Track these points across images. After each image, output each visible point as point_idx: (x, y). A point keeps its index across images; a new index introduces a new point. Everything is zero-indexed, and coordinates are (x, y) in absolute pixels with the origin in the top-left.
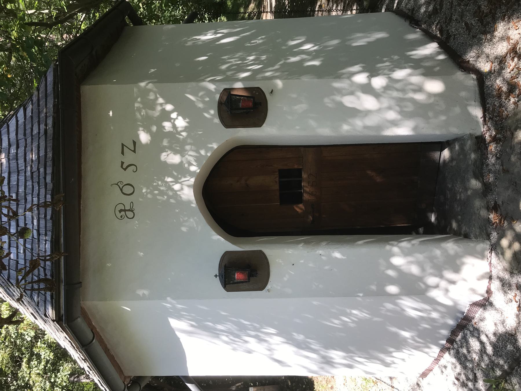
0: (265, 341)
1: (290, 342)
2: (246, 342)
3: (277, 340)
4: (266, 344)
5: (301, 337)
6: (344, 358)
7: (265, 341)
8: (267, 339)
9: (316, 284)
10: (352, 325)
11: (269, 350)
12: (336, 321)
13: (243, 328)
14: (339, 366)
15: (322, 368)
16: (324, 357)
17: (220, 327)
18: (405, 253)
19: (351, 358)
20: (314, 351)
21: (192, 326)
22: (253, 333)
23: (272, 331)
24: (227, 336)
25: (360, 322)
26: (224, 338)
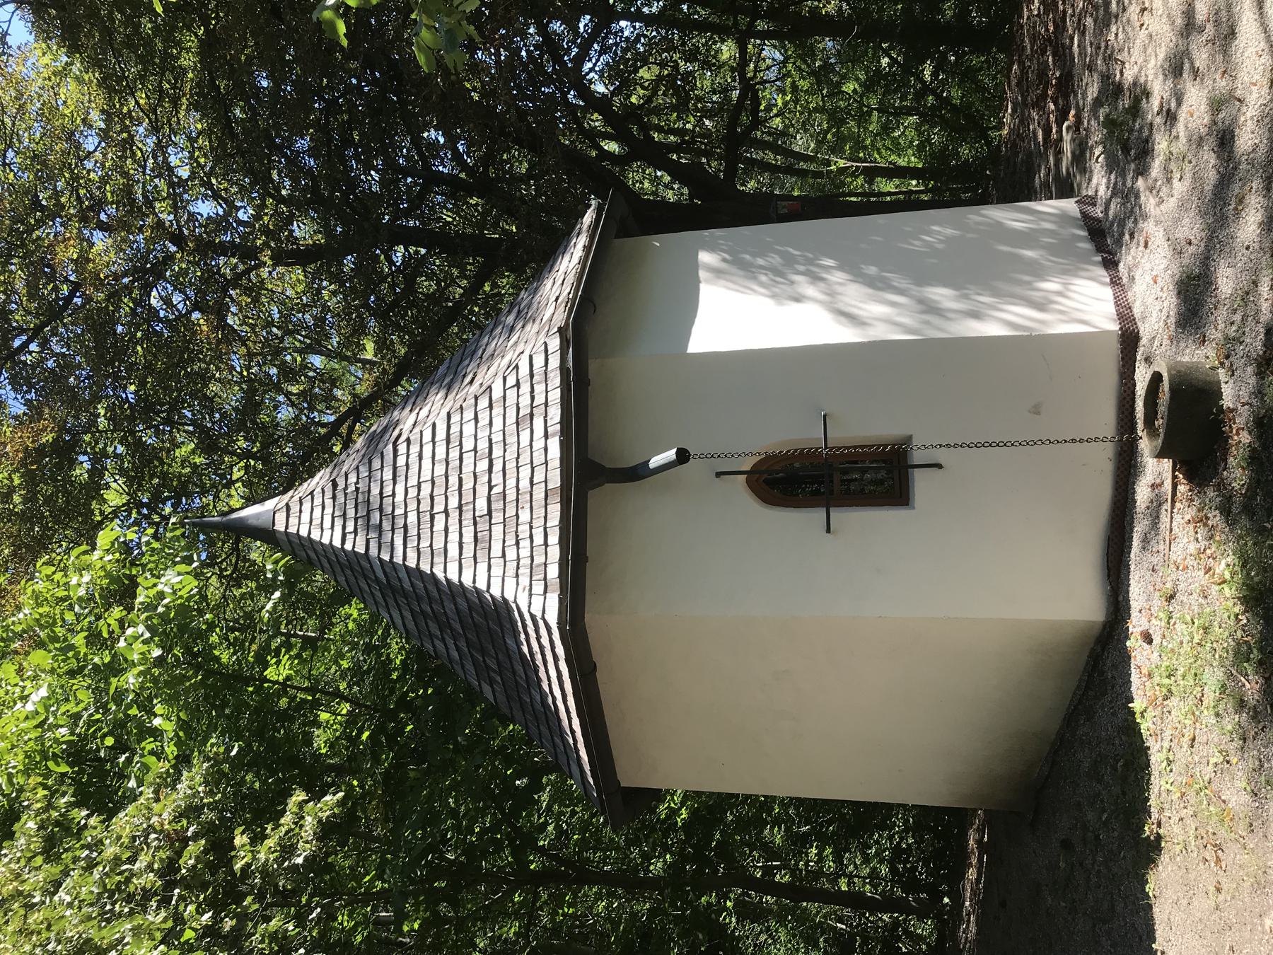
0: (822, 279)
1: (860, 280)
2: (792, 283)
3: (838, 277)
4: (822, 285)
5: (872, 270)
6: (957, 298)
7: (822, 279)
8: (825, 276)
9: (17, 482)
10: (940, 246)
11: (828, 294)
12: (916, 243)
13: (790, 261)
14: (875, 323)
15: (927, 323)
16: (921, 301)
17: (760, 261)
18: (712, 248)
19: (966, 297)
20: (901, 292)
21: (724, 260)
22: (801, 268)
23: (829, 262)
24: (766, 274)
25: (948, 240)
26: (763, 278)
